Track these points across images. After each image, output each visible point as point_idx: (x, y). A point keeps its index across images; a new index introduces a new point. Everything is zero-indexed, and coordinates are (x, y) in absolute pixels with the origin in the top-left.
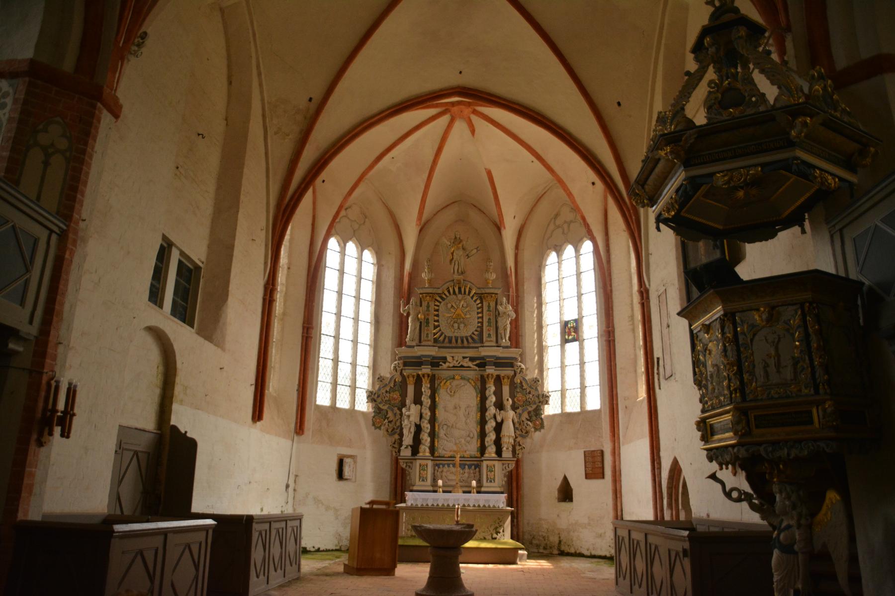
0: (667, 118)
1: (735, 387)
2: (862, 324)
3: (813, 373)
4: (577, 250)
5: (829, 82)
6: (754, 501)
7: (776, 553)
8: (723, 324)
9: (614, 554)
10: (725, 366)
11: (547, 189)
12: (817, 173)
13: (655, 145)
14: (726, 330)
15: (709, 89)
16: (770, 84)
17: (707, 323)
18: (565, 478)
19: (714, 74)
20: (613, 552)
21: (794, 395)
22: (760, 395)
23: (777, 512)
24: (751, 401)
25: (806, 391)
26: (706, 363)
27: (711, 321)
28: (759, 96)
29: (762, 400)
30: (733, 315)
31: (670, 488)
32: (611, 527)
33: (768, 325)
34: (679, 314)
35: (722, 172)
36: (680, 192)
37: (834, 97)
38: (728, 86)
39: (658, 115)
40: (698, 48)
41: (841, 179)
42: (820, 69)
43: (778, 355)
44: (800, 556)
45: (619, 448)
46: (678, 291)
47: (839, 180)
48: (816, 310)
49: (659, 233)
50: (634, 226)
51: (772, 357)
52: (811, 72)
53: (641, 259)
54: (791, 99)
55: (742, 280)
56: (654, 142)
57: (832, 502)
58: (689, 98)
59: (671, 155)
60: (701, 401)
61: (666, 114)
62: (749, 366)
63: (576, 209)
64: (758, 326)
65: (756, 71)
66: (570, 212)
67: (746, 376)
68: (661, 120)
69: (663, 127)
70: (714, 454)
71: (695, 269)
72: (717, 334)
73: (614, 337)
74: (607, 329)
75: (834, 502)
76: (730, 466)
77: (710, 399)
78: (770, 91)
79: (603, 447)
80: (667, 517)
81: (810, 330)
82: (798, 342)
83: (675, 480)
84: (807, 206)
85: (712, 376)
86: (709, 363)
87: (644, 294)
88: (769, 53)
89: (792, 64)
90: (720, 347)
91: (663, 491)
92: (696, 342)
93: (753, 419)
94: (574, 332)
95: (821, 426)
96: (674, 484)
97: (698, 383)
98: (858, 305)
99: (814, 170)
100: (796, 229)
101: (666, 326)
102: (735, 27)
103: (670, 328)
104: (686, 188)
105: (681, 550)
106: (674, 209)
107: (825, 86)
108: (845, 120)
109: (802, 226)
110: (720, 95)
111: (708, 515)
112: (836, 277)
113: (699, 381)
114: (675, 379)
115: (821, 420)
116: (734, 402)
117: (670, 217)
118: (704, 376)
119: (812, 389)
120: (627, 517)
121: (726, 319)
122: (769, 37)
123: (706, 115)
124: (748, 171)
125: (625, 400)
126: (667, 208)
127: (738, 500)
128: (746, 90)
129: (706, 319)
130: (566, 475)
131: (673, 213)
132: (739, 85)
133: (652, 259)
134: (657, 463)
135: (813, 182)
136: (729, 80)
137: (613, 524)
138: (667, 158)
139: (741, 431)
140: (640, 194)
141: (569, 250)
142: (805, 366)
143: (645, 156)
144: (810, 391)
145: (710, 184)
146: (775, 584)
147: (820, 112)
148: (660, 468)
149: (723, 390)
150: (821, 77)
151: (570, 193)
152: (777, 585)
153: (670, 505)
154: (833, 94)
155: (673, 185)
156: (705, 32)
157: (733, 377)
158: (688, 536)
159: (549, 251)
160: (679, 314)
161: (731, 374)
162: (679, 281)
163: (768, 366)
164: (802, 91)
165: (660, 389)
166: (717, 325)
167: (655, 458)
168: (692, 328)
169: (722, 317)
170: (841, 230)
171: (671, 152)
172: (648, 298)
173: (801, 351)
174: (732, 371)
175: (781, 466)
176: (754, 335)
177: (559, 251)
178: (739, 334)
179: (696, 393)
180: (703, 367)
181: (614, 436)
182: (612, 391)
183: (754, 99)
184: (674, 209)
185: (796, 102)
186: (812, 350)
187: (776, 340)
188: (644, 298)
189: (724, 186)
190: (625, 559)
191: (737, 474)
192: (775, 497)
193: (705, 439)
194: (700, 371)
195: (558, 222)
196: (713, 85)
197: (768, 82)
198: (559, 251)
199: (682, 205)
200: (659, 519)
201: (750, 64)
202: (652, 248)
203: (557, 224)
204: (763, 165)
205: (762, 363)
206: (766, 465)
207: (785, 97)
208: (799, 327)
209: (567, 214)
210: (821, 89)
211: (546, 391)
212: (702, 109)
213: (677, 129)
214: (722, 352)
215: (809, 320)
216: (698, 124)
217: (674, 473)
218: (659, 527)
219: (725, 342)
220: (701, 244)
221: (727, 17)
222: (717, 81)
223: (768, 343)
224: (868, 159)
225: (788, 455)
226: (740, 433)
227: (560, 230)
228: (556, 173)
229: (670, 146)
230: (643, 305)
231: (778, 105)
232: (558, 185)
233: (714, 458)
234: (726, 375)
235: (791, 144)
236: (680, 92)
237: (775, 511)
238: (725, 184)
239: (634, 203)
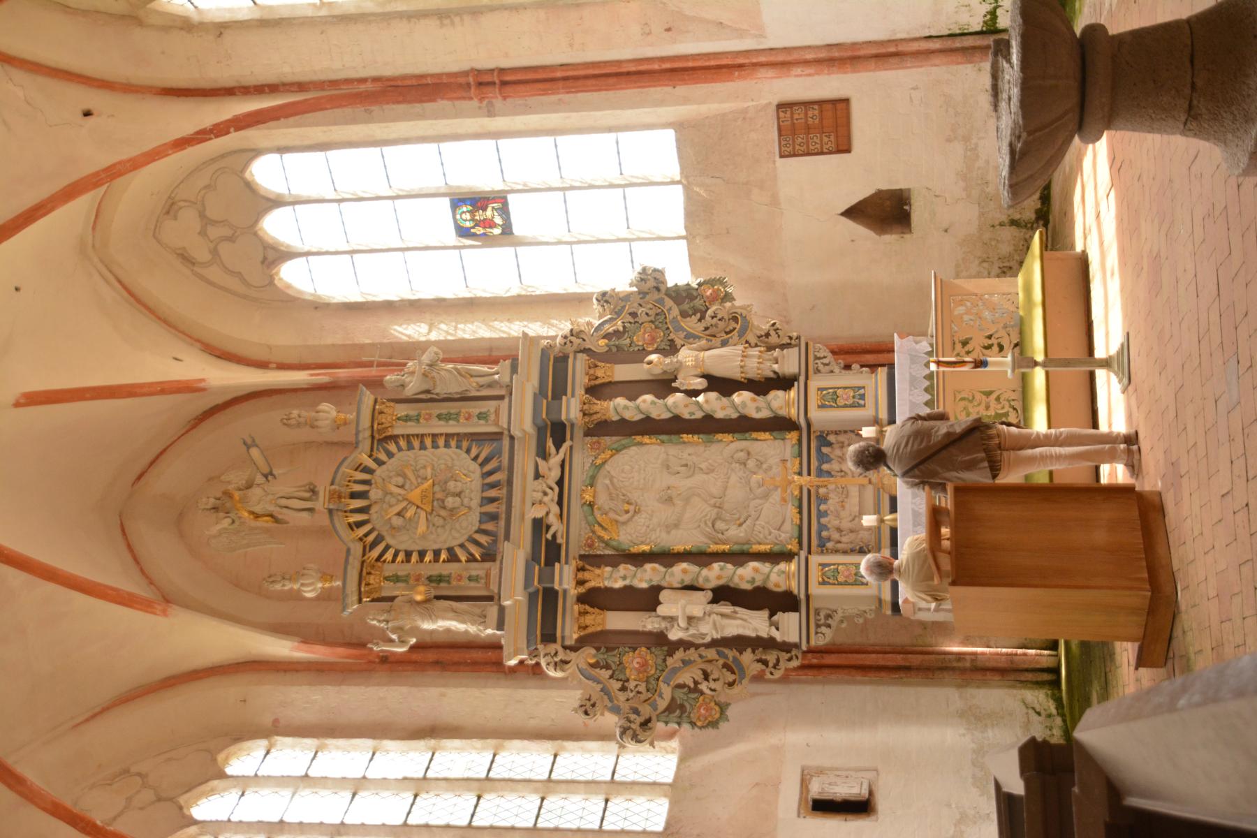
4: (276, 202)
66: (175, 218)
94: (484, 209)
141: (275, 226)
181: (741, 66)
182: (628, 74)
195: (202, 254)
198: (276, 255)
227: (225, 249)
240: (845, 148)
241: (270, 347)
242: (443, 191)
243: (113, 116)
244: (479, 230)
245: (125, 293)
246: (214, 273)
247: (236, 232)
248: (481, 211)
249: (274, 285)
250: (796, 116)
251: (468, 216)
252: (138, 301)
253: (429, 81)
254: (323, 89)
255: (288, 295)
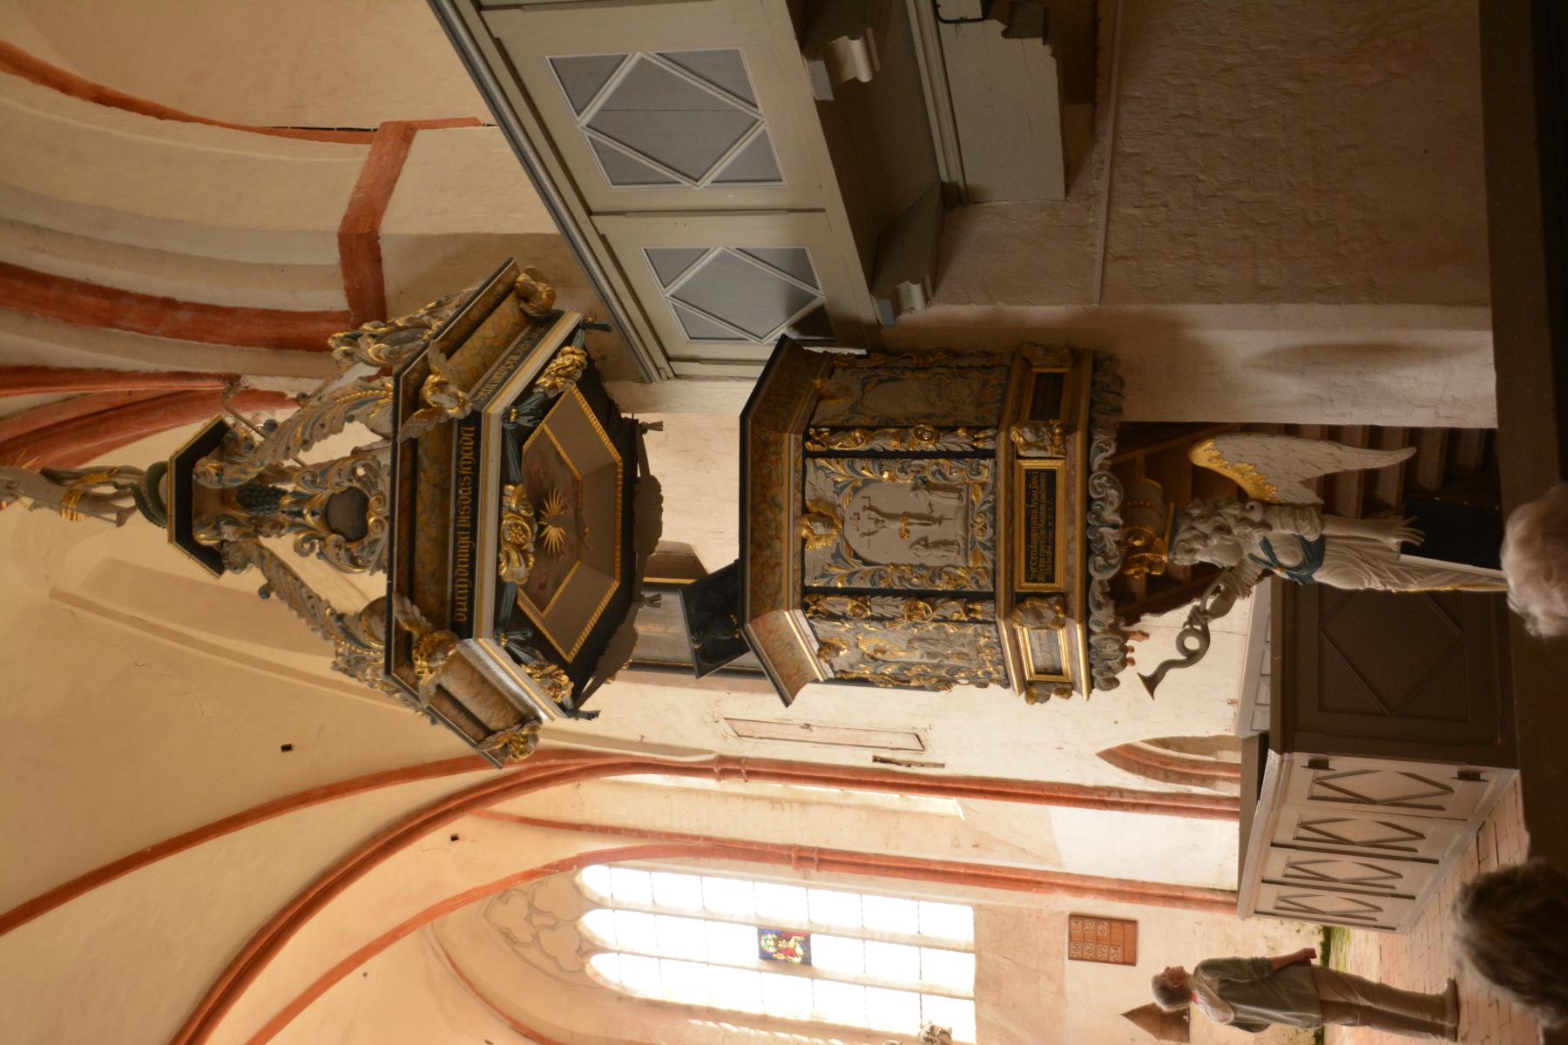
0: (352, 653)
1: (961, 610)
2: (863, 352)
3: (949, 455)
4: (598, 904)
5: (366, 326)
6: (1208, 607)
7: (1320, 577)
8: (823, 614)
9: (1319, 925)
10: (915, 625)
11: (440, 951)
12: (545, 382)
13: (406, 688)
14: (837, 610)
15: (313, 555)
16: (339, 435)
17: (816, 646)
18: (1133, 1015)
19: (283, 538)
20: (1311, 926)
21: (991, 498)
22: (985, 564)
23: (1234, 564)
24: (994, 583)
25: (986, 473)
26: (903, 662)
27: (812, 637)
28: (356, 461)
29: (994, 562)
30: (806, 591)
31: (1167, 777)
32: (1253, 921)
33: (841, 526)
34: (787, 703)
35: (498, 562)
36: (522, 655)
37: (400, 324)
38: (317, 517)
39: (340, 670)
40: (214, 559)
41: (568, 341)
42: (334, 338)
43: (907, 515)
44: (1327, 532)
45: (1068, 875)
46: (734, 694)
47: (570, 345)
48: (823, 430)
49: (600, 715)
50: (573, 763)
51: (908, 527)
52: (337, 354)
53: (649, 762)
54: (381, 401)
55: (736, 561)
56: (397, 691)
57: (1218, 458)
58: (320, 600)
59: (436, 660)
60: (985, 685)
61: (342, 655)
62: (920, 577)
63: (502, 889)
64: (838, 544)
65: (302, 456)
66: (507, 903)
67: (941, 586)
68: (351, 666)
69: (368, 665)
70: (1102, 674)
71: (696, 652)
72: (843, 630)
73: (812, 850)
74: (793, 862)
75: (1216, 453)
76: (1130, 643)
77: (982, 665)
78: (356, 435)
79: (1063, 912)
80: (1234, 791)
81: (863, 447)
82: (882, 473)
83: (1148, 762)
84: (607, 411)
85: (930, 655)
86: (903, 656)
87: (726, 767)
88: (271, 425)
89: (309, 386)
90: (873, 629)
91: (1173, 791)
92: (854, 676)
93: (1035, 585)
94: (788, 939)
95: (1060, 456)
96: (1157, 764)
97: (945, 683)
98: (825, 352)
99: (538, 386)
100: (649, 438)
101: (805, 730)
102: (194, 477)
103: (811, 723)
104: (517, 642)
105: (1312, 771)
106: (557, 675)
107: (373, 336)
108: (451, 314)
109: (645, 428)
110: (334, 536)
111: (1232, 702)
112: (762, 381)
113: (939, 681)
114: (926, 730)
115: (1049, 455)
116: (994, 617)
117: (572, 685)
118: (929, 670)
119: (982, 462)
120: (1231, 881)
121: (814, 607)
122: (238, 417)
123: (368, 572)
124: (510, 510)
125: (958, 846)
126: (550, 689)
127: (1205, 636)
128: (337, 484)
129: (807, 648)
130: (1122, 1012)
131: (565, 678)
132: (323, 495)
133: (654, 737)
134: (1109, 795)
135: (562, 393)
136: (305, 512)
137: (1245, 916)
138: (440, 670)
139: (1057, 612)
140: (506, 741)
141: (593, 923)
142: (935, 468)
143: (423, 715)
144: (985, 467)
145: (521, 591)
146: (1389, 588)
147: (423, 355)
148: (1121, 792)
149: (965, 636)
150: (353, 340)
151: (462, 896)
152: (1391, 584)
153: (1205, 781)
154: (393, 324)
155: (501, 666)
156: (184, 538)
157: (941, 611)
158: (1281, 752)
159: (587, 970)
160: (787, 703)
161: (934, 615)
162: (712, 689)
163: (925, 539)
164: (370, 379)
165: (943, 765)
166: (824, 627)
167: (1097, 798)
168: (821, 679)
169: (808, 615)
170: (669, 359)
171: (430, 658)
172: (737, 760)
173: (903, 470)
174: (927, 612)
175: (1137, 543)
176: (856, 556)
177: (592, 943)
178: (852, 586)
179: (964, 692)
180: (908, 669)
181: (1039, 883)
182: (935, 872)
183: (361, 472)
184: (557, 675)
185: (391, 393)
186: (902, 450)
187: (873, 515)
188: (737, 768)
189: (531, 564)
190: (1332, 902)
191: (1146, 631)
192: (1202, 564)
193: (1066, 690)
194: (918, 676)
195: (524, 936)
196: (307, 546)
197: (332, 437)
198: (588, 947)
199: (551, 656)
200: (1238, 810)
201: (282, 464)
202: (631, 735)
203: (528, 939)
204: (505, 479)
205: (917, 549)
206: (1132, 571)
207: (373, 412)
208: (851, 467)
209: (511, 913)
210: (376, 343)
211: (919, 1030)
212: (350, 577)
213: (383, 637)
214: (884, 626)
215: (840, 446)
216: (383, 592)
217: (1135, 761)
218: (1256, 813)
219: (864, 617)
220: (641, 628)
221: (167, 488)
222: (301, 536)
223: (876, 532)
224: (540, 288)
225: (1114, 526)
226: (1061, 616)
227: (545, 936)
228: (407, 922)
229: (417, 659)
230: (752, 774)
231: (387, 428)
232: (436, 922)
233: (1111, 675)
234: (934, 624)
235: (474, 420)
236: (301, 615)
237: (1232, 568)
238: (527, 561)
239: (524, 757)
240: (1130, 961)
241: (572, 1033)
242: (751, 921)
243: (475, 841)
244: (781, 957)
245: (451, 969)
246: (532, 954)
247: (558, 923)
248: (784, 941)
249: (584, 972)
250: (1087, 928)
251: (772, 943)
252: (462, 975)
253: (755, 848)
254: (659, 839)
255: (595, 983)
